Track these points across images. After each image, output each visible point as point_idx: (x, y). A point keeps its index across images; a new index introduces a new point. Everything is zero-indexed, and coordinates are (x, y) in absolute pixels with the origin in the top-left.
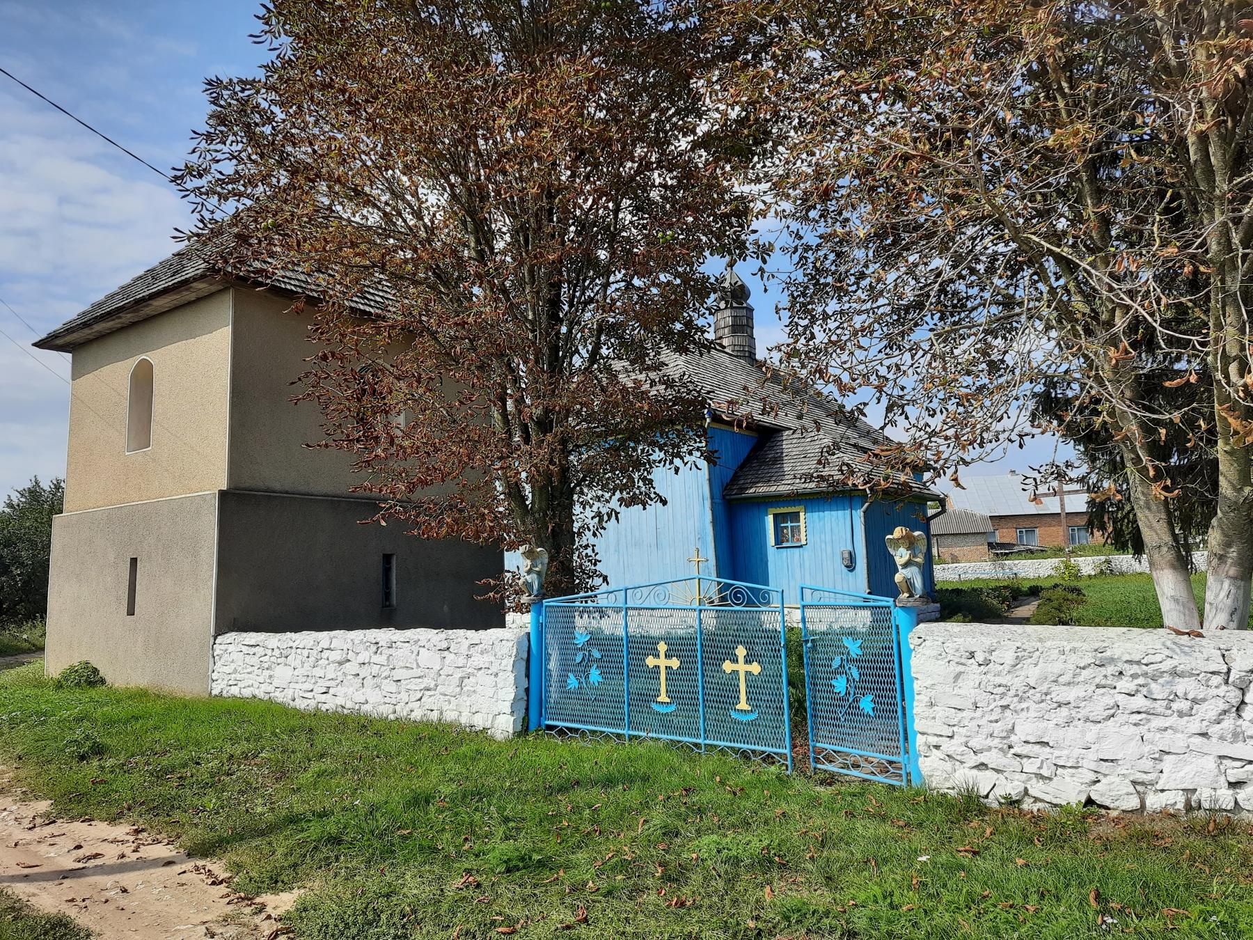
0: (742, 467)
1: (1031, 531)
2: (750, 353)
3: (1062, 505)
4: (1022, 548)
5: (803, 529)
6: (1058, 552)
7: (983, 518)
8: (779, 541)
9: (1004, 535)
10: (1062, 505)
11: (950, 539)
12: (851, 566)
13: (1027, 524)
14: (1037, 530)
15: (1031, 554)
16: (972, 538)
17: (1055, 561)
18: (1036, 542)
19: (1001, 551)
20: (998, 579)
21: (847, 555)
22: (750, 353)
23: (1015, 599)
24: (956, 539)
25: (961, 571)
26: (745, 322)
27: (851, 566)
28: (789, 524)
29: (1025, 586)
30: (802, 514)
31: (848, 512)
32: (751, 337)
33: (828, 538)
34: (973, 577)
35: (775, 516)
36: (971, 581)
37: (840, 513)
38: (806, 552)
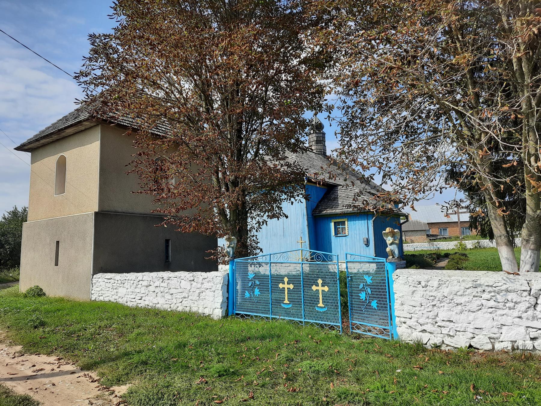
0: (320, 202)
1: (445, 229)
2: (324, 152)
3: (459, 218)
4: (441, 237)
5: (347, 229)
6: (457, 238)
7: (424, 224)
8: (336, 234)
9: (434, 231)
10: (459, 218)
11: (410, 233)
12: (367, 245)
13: (443, 226)
14: (448, 229)
15: (445, 239)
16: (420, 233)
17: (455, 242)
18: (447, 234)
19: (432, 238)
20: (431, 250)
21: (365, 240)
22: (324, 152)
23: (438, 259)
24: (413, 233)
25: (415, 247)
26: (322, 139)
27: (367, 245)
28: (341, 226)
29: (443, 253)
30: (346, 222)
31: (366, 221)
32: (324, 145)
33: (358, 232)
34: (420, 249)
35: (335, 223)
36: (419, 251)
37: (363, 221)
38: (348, 239)
